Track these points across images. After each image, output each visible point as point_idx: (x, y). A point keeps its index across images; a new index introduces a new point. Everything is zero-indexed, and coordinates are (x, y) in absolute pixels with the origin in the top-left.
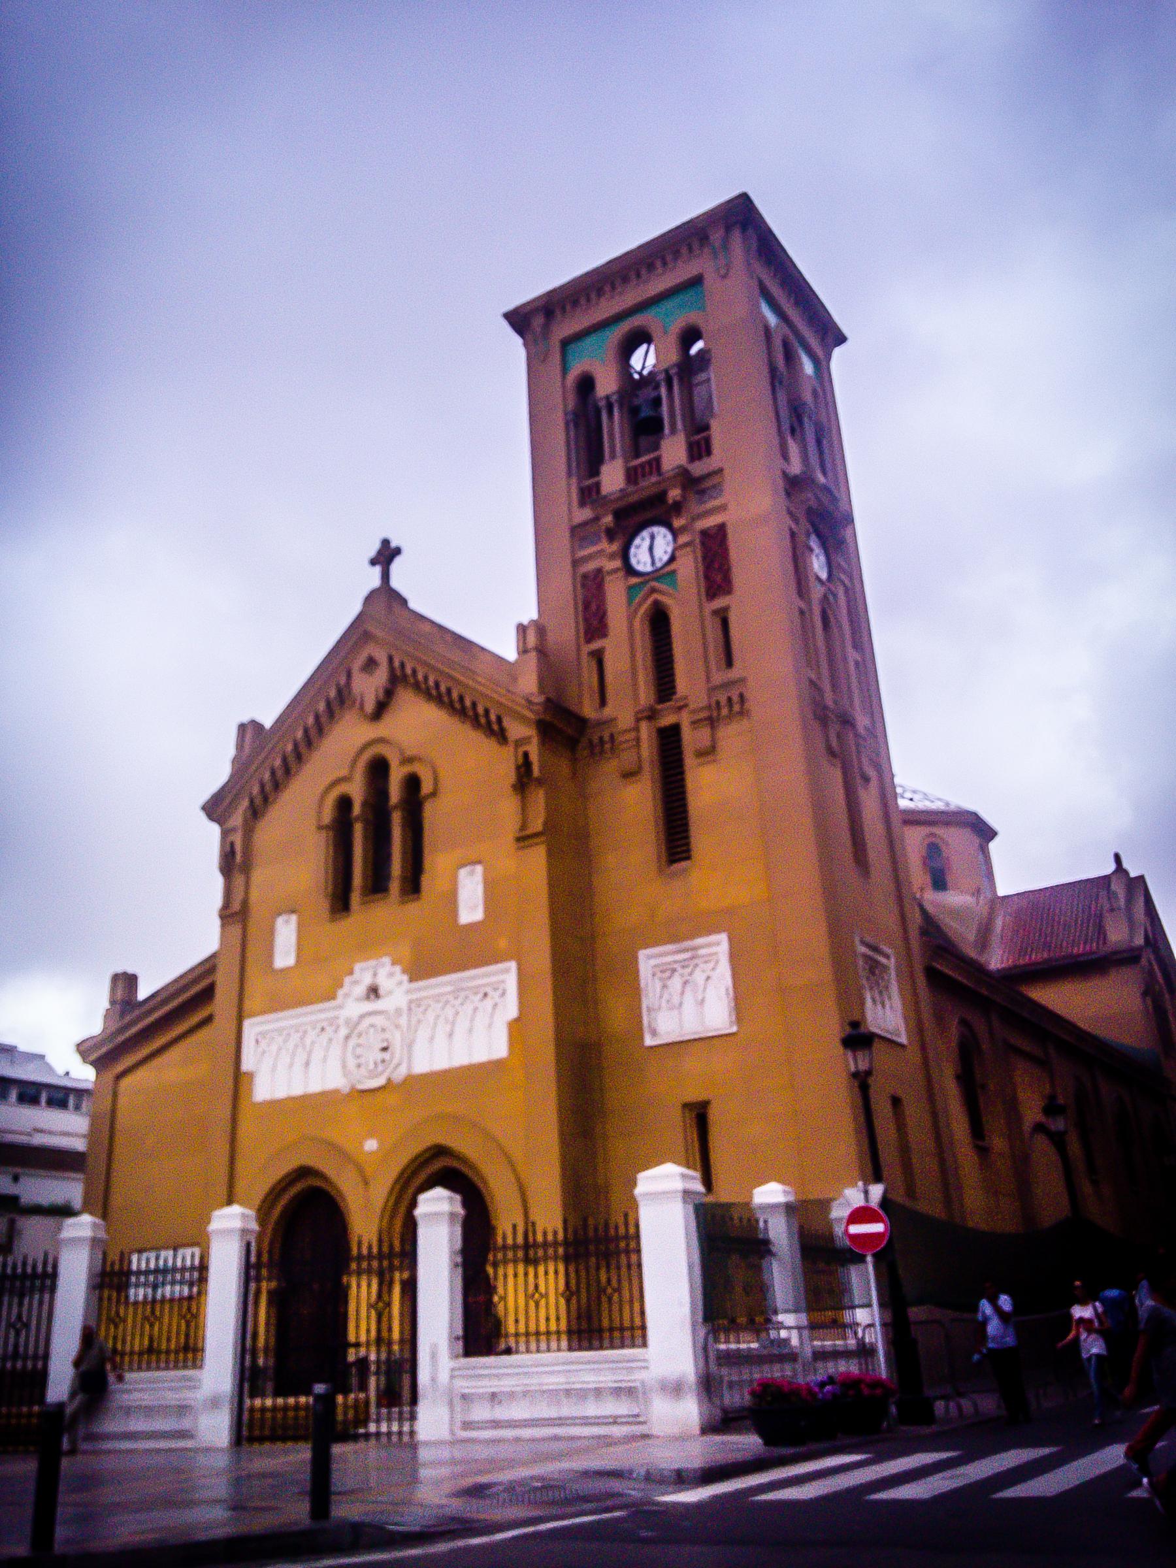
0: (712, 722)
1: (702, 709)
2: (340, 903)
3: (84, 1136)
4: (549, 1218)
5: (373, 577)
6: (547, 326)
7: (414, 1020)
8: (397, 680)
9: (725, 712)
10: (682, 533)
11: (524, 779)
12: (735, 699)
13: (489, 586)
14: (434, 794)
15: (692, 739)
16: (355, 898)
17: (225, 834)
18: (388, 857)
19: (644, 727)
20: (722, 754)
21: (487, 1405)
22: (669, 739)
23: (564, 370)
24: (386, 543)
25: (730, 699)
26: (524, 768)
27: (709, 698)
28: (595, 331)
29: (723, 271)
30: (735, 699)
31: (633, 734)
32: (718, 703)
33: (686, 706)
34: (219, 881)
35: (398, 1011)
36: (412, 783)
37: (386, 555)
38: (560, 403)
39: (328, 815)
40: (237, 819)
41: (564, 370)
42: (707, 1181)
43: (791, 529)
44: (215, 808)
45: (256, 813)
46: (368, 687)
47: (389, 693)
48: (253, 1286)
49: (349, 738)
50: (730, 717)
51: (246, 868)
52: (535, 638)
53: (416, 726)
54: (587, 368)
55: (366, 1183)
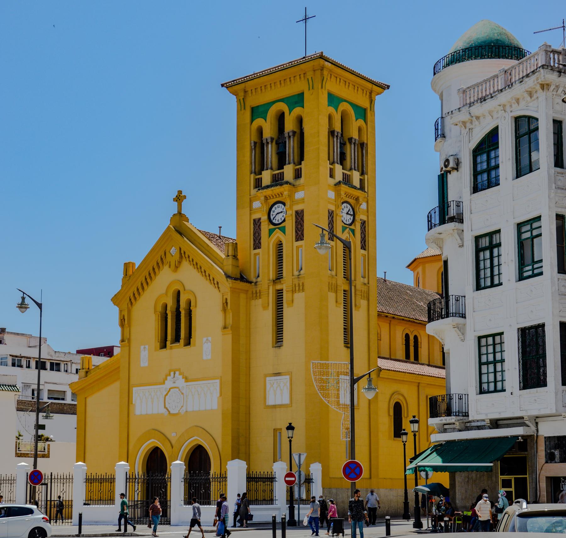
0: (293, 291)
2: (164, 346)
3: (40, 358)
4: (493, 380)
13: (219, 213)
15: (286, 297)
16: (168, 343)
17: (121, 311)
18: (180, 329)
22: (279, 295)
24: (180, 192)
28: (176, 329)
34: (119, 329)
37: (179, 198)
38: (249, 139)
39: (160, 309)
40: (125, 306)
44: (116, 300)
47: (180, 262)
48: (128, 484)
49: (164, 281)
53: (190, 279)
55: (172, 447)
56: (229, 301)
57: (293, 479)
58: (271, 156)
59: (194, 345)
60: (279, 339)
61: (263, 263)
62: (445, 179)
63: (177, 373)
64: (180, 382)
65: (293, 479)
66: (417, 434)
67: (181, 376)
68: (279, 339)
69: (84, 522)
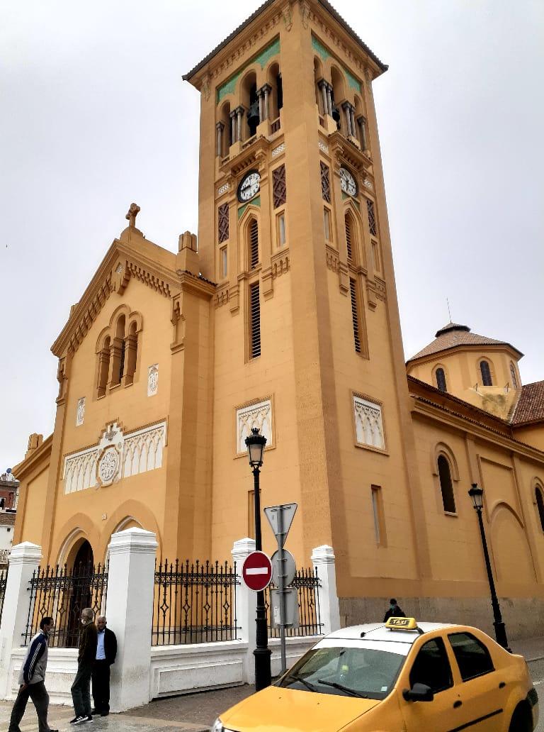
0: (273, 276)
1: (268, 270)
5: (127, 223)
6: (209, 82)
7: (126, 448)
8: (129, 274)
9: (279, 269)
10: (263, 173)
11: (176, 318)
12: (284, 261)
13: (174, 216)
14: (141, 330)
15: (262, 289)
17: (61, 360)
19: (242, 283)
20: (276, 293)
21: (507, 680)
22: (254, 288)
23: (218, 100)
25: (281, 262)
26: (176, 311)
27: (272, 263)
29: (289, 28)
30: (284, 261)
31: (236, 289)
32: (276, 265)
33: (261, 269)
34: (58, 384)
35: (120, 445)
36: (134, 325)
37: (134, 212)
40: (65, 354)
41: (218, 100)
42: (259, 546)
43: (322, 164)
45: (73, 350)
46: (118, 276)
47: (127, 281)
50: (282, 271)
51: (258, 399)
52: (188, 242)
54: (226, 99)
56: (181, 306)
57: (264, 571)
58: (241, 127)
59: (138, 381)
60: (255, 348)
61: (230, 266)
62: (360, 446)
63: (115, 425)
64: (119, 438)
65: (264, 571)
66: (482, 510)
67: (119, 429)
68: (255, 348)
69: (23, 658)
